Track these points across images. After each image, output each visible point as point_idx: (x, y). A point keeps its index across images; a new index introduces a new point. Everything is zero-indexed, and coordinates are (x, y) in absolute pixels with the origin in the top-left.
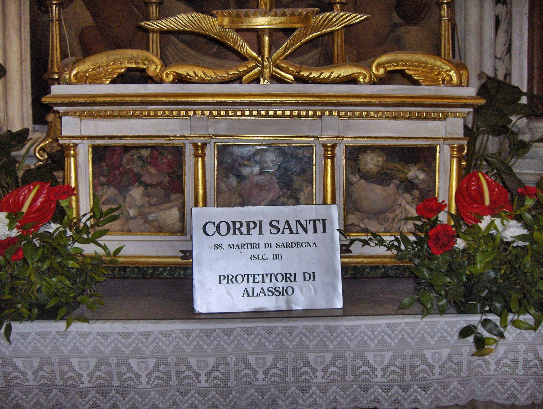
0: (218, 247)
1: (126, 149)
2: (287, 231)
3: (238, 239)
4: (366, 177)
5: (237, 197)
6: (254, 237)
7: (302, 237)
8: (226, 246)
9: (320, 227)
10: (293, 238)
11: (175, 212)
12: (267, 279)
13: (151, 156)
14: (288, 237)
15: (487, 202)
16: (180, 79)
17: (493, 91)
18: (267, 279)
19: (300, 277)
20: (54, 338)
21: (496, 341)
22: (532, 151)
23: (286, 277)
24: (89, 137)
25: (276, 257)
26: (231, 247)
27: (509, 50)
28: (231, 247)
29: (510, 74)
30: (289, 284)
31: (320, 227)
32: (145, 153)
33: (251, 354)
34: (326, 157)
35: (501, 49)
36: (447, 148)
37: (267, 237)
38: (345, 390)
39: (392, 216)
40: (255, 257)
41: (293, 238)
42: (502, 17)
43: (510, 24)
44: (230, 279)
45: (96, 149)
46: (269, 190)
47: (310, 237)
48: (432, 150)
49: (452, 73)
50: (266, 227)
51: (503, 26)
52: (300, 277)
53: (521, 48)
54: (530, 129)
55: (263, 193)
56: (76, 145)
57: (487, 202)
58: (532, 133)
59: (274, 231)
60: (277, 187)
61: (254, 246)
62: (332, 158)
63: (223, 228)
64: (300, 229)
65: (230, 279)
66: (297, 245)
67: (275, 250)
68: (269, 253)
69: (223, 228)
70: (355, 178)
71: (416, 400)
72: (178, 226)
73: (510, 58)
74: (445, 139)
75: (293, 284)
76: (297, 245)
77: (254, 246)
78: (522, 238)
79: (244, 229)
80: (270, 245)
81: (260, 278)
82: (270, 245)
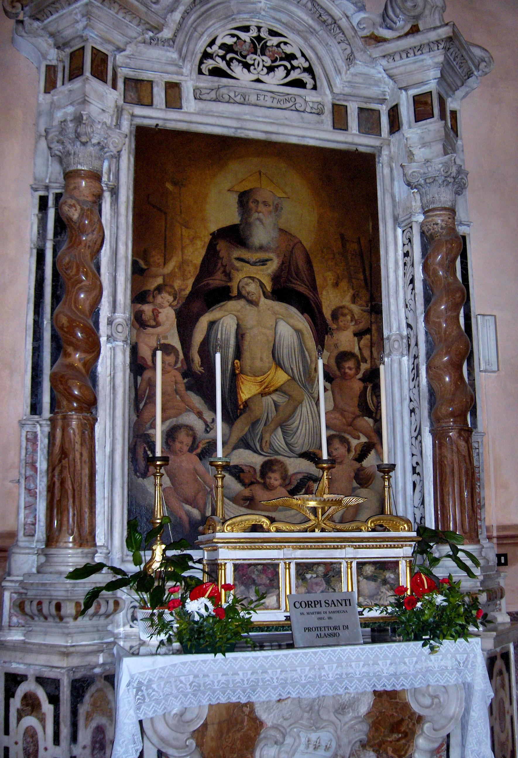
0: (302, 614)
1: (250, 565)
2: (333, 605)
3: (311, 610)
4: (367, 578)
5: (488, 563)
6: (318, 609)
7: (340, 608)
8: (305, 613)
9: (348, 603)
10: (337, 609)
11: (275, 598)
12: (326, 629)
13: (263, 570)
14: (333, 608)
15: (426, 587)
16: (278, 530)
17: (421, 531)
18: (326, 629)
19: (341, 628)
20: (231, 661)
21: (438, 647)
22: (441, 563)
23: (335, 628)
24: (233, 559)
25: (330, 618)
26: (308, 613)
27: (423, 503)
28: (308, 613)
29: (424, 518)
30: (337, 631)
31: (348, 603)
32: (259, 567)
33: (326, 664)
34: (286, 568)
35: (417, 502)
36: (404, 562)
37: (324, 609)
38: (369, 681)
39: (379, 597)
40: (320, 619)
41: (337, 609)
42: (418, 483)
43: (422, 487)
44: (309, 629)
45: (235, 565)
46: (320, 586)
47: (344, 608)
48: (397, 563)
49: (405, 525)
50: (323, 604)
51: (418, 488)
52: (341, 628)
53: (430, 502)
54: (438, 550)
55: (318, 587)
56: (226, 563)
57: (426, 587)
58: (440, 553)
59: (327, 605)
60: (324, 583)
61: (319, 613)
62: (289, 569)
63: (303, 605)
64: (339, 604)
65: (309, 629)
66: (338, 612)
67: (328, 615)
68: (326, 616)
69: (303, 605)
70: (361, 579)
71: (403, 685)
72: (276, 606)
73: (424, 507)
74: (404, 557)
75: (339, 631)
76: (338, 612)
77: (319, 613)
78: (444, 600)
79: (313, 605)
80: (326, 612)
81: (323, 629)
82: (326, 612)
